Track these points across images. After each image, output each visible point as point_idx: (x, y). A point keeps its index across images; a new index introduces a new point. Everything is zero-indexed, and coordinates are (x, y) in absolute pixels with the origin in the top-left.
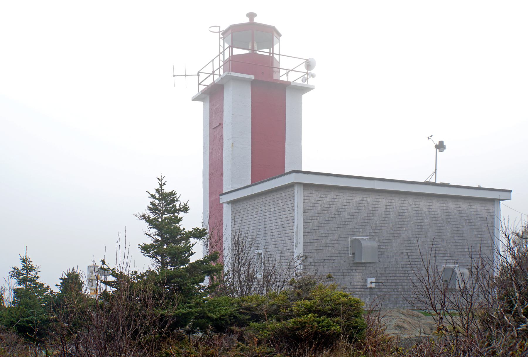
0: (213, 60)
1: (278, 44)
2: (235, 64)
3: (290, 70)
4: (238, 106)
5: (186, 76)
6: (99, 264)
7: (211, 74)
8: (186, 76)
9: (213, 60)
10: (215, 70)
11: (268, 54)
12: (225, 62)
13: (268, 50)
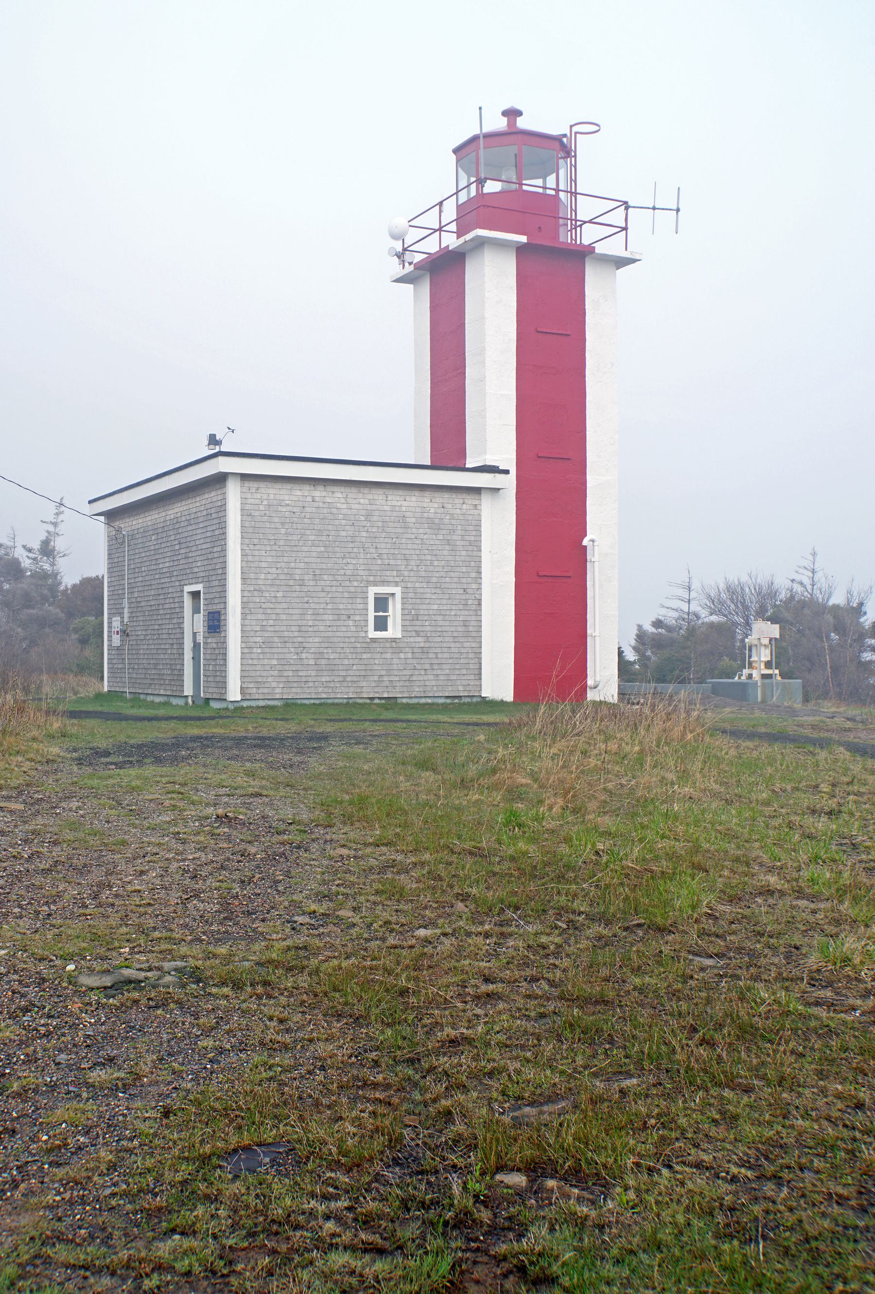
0: (441, 204)
1: (554, 175)
2: (474, 213)
3: (585, 222)
4: (493, 294)
5: (654, 208)
6: (497, 123)
7: (436, 231)
8: (654, 208)
9: (441, 204)
10: (460, 188)
11: (540, 190)
12: (18, 559)
13: (539, 182)
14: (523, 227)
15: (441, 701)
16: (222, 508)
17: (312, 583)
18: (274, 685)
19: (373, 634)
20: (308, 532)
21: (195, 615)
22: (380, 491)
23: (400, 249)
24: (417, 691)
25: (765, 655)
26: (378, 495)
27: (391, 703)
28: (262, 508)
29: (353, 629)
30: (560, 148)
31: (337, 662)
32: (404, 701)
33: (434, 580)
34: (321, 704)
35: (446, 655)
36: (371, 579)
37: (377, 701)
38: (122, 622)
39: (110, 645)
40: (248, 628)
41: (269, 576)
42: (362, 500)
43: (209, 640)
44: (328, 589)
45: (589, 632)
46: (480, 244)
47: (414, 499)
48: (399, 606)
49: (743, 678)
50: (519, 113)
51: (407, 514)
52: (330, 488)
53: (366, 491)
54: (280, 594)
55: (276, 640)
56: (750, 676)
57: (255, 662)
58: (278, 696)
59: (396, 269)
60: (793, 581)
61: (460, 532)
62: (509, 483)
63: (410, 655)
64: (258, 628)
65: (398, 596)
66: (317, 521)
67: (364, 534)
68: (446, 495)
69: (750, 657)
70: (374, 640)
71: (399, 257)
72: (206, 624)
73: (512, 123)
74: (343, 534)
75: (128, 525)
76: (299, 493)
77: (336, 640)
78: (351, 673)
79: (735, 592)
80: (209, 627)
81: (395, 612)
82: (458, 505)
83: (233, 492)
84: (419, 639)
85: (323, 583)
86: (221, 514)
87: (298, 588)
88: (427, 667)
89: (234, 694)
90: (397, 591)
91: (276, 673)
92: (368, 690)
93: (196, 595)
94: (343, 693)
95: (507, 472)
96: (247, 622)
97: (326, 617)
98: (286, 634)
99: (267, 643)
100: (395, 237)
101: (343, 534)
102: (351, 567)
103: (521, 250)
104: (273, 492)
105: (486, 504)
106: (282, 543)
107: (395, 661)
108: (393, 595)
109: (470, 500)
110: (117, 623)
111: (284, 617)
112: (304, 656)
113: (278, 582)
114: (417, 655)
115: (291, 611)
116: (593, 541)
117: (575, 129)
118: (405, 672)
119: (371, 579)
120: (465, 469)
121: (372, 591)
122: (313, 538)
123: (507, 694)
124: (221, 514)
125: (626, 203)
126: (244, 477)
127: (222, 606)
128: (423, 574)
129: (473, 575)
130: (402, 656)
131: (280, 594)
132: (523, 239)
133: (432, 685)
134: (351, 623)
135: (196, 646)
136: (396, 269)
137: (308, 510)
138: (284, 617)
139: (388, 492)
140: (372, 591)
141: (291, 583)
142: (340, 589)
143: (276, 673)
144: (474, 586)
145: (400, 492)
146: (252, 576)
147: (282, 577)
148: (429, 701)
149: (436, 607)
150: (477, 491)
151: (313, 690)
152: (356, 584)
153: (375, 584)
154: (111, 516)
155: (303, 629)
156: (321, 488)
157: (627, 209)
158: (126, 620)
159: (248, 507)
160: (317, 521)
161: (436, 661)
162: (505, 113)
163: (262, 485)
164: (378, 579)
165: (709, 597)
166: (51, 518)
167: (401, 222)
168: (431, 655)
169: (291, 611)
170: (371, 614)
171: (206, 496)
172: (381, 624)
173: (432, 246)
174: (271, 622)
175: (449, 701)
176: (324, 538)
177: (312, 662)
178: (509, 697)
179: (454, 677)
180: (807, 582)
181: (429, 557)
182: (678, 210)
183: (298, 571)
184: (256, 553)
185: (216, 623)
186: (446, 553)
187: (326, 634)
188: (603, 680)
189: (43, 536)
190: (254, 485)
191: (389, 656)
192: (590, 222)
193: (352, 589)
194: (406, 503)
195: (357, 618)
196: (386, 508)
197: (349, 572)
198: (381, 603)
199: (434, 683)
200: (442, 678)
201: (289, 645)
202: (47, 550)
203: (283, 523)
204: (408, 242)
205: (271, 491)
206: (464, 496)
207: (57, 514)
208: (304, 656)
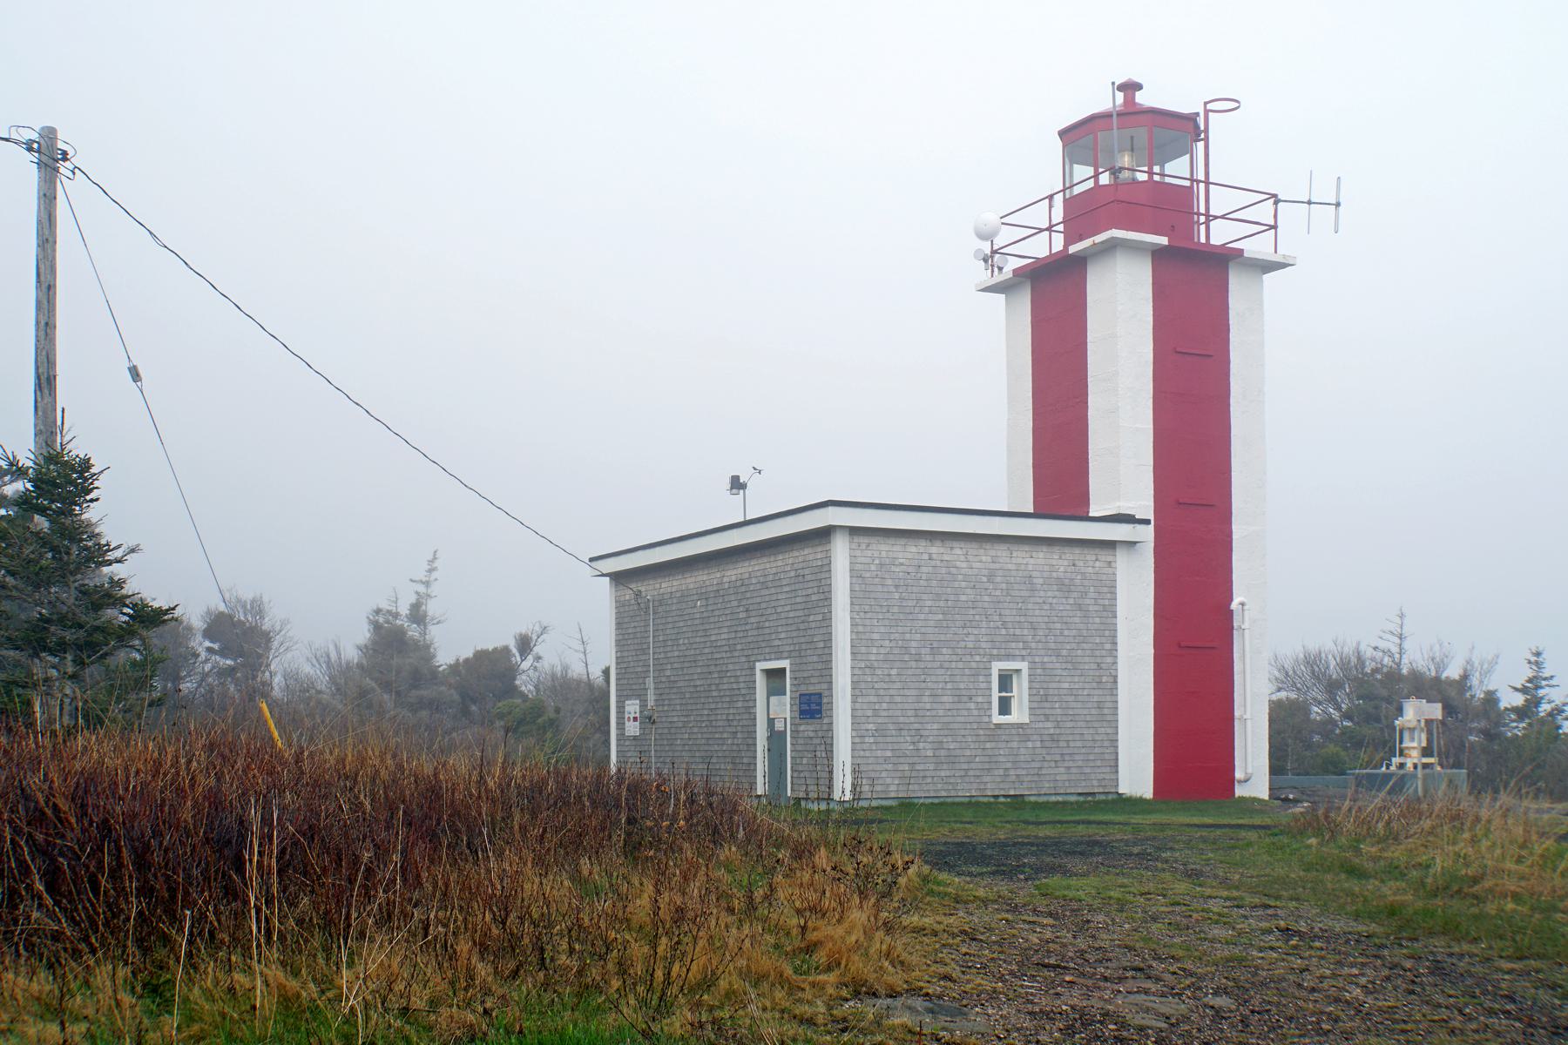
0: (1051, 197)
7: (1041, 230)
8: (1309, 203)
9: (1051, 197)
14: (1141, 226)
15: (1073, 799)
16: (826, 567)
17: (928, 658)
18: (889, 781)
19: (998, 719)
20: (925, 597)
21: (773, 699)
22: (1003, 547)
23: (988, 252)
24: (1046, 787)
25: (1422, 739)
26: (1001, 551)
27: (1017, 802)
28: (873, 568)
29: (975, 713)
30: (1183, 130)
31: (958, 752)
32: (1033, 799)
33: (1064, 653)
34: (941, 804)
35: (1079, 744)
36: (995, 652)
37: (1002, 800)
38: (643, 706)
39: (621, 736)
40: (859, 713)
41: (882, 651)
42: (983, 558)
43: (802, 728)
44: (946, 665)
45: (1237, 714)
46: (1112, 246)
47: (1041, 555)
48: (1025, 684)
49: (1393, 768)
50: (1139, 87)
51: (1034, 574)
52: (949, 544)
53: (988, 546)
54: (894, 672)
55: (891, 727)
56: (1402, 766)
57: (867, 754)
58: (893, 795)
59: (984, 276)
60: (1375, 648)
61: (1092, 595)
62: (1147, 534)
63: (1038, 744)
64: (869, 713)
65: (1025, 673)
66: (934, 583)
67: (986, 598)
68: (1077, 551)
69: (1401, 742)
70: (998, 726)
71: (985, 261)
72: (796, 708)
73: (1129, 101)
74: (963, 598)
75: (651, 589)
76: (914, 549)
77: (956, 726)
78: (973, 766)
79: (1313, 663)
80: (802, 712)
81: (1021, 692)
82: (1090, 562)
83: (841, 550)
84: (1049, 725)
85: (941, 658)
86: (823, 575)
87: (913, 664)
88: (1058, 758)
89: (843, 787)
90: (1023, 666)
91: (890, 767)
92: (992, 786)
93: (775, 675)
94: (965, 790)
95: (1147, 522)
96: (858, 706)
97: (945, 699)
98: (901, 719)
99: (880, 731)
100: (982, 236)
101: (963, 598)
102: (972, 638)
103: (1158, 254)
104: (884, 548)
105: (1121, 559)
106: (896, 610)
107: (1023, 751)
108: (1018, 671)
109: (1105, 556)
110: (632, 707)
111: (898, 699)
112: (921, 745)
113: (891, 657)
114: (1048, 744)
115: (907, 692)
116: (1243, 604)
117: (1209, 107)
118: (1034, 765)
119: (995, 652)
120: (1087, 518)
121: (997, 667)
122: (929, 603)
123: (1146, 790)
124: (823, 575)
125: (1275, 196)
126: (854, 531)
127: (825, 686)
128: (1052, 646)
129: (1108, 646)
130: (1030, 744)
131: (894, 672)
132: (1164, 241)
133: (1059, 780)
134: (972, 706)
135: (776, 738)
136: (984, 276)
137: (924, 569)
138: (898, 699)
139: (1014, 547)
140: (997, 667)
141: (906, 658)
142: (960, 665)
143: (890, 767)
144: (1109, 660)
145: (1027, 548)
146: (863, 650)
147: (896, 651)
148: (1060, 799)
149: (1066, 685)
150: (1110, 545)
151: (931, 787)
152: (978, 658)
153: (999, 658)
154: (618, 578)
155: (920, 713)
156: (938, 543)
157: (1276, 203)
158: (651, 703)
159: (858, 567)
160: (934, 583)
161: (1066, 751)
162: (1122, 87)
163: (873, 540)
164: (1003, 652)
165: (1282, 669)
166: (422, 575)
167: (992, 218)
168: (1062, 744)
169: (907, 692)
170: (996, 695)
171: (796, 554)
172: (1005, 707)
173: (1039, 248)
174: (885, 706)
175: (1081, 799)
176: (942, 604)
177: (930, 753)
178: (1148, 794)
179: (1088, 770)
180: (1395, 649)
181: (1058, 626)
182: (1338, 205)
183: (914, 644)
184: (868, 622)
185: (813, 707)
186: (1077, 620)
187: (946, 720)
188: (1253, 770)
189: (413, 599)
190: (864, 540)
191: (1015, 745)
192: (1223, 217)
193: (974, 665)
194: (1032, 561)
195: (980, 699)
196: (1010, 566)
197: (970, 645)
198: (1005, 680)
199: (1065, 777)
200: (1074, 770)
201: (904, 733)
202: (418, 615)
203: (897, 586)
204: (998, 243)
205: (884, 547)
206: (1097, 551)
207: (430, 571)
208: (921, 745)
